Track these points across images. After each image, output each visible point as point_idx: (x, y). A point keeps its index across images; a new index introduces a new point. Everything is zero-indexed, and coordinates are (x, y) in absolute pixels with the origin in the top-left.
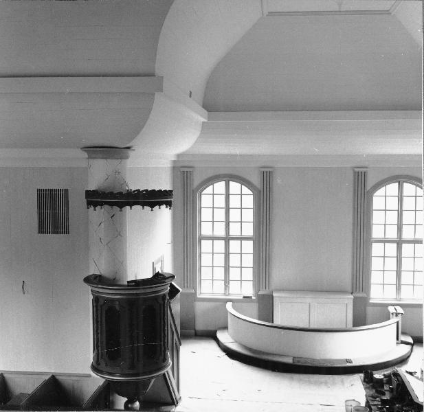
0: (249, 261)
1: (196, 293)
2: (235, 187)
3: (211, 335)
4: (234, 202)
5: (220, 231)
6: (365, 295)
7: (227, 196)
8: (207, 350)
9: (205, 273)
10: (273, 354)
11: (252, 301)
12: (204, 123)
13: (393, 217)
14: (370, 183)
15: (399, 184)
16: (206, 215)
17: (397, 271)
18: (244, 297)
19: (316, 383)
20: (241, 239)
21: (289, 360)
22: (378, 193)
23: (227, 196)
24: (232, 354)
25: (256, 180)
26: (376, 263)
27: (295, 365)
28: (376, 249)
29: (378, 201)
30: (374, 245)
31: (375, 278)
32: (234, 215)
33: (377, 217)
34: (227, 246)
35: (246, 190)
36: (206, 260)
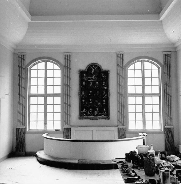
0: (58, 109)
1: (26, 128)
2: (50, 65)
3: (33, 154)
4: (147, 73)
5: (148, 100)
6: (124, 127)
7: (46, 70)
8: (31, 162)
9: (33, 117)
10: (65, 159)
11: (60, 133)
12: (29, 23)
13: (139, 81)
14: (126, 61)
15: (142, 62)
16: (33, 82)
17: (143, 113)
18: (56, 130)
19: (91, 174)
20: (54, 95)
21: (76, 161)
22: (130, 68)
23: (46, 70)
24: (43, 162)
25: (62, 61)
26: (131, 109)
27: (80, 164)
28: (131, 100)
29: (130, 72)
30: (129, 97)
31: (131, 117)
32: (50, 82)
33: (130, 81)
34: (45, 100)
35: (56, 67)
36: (33, 109)
